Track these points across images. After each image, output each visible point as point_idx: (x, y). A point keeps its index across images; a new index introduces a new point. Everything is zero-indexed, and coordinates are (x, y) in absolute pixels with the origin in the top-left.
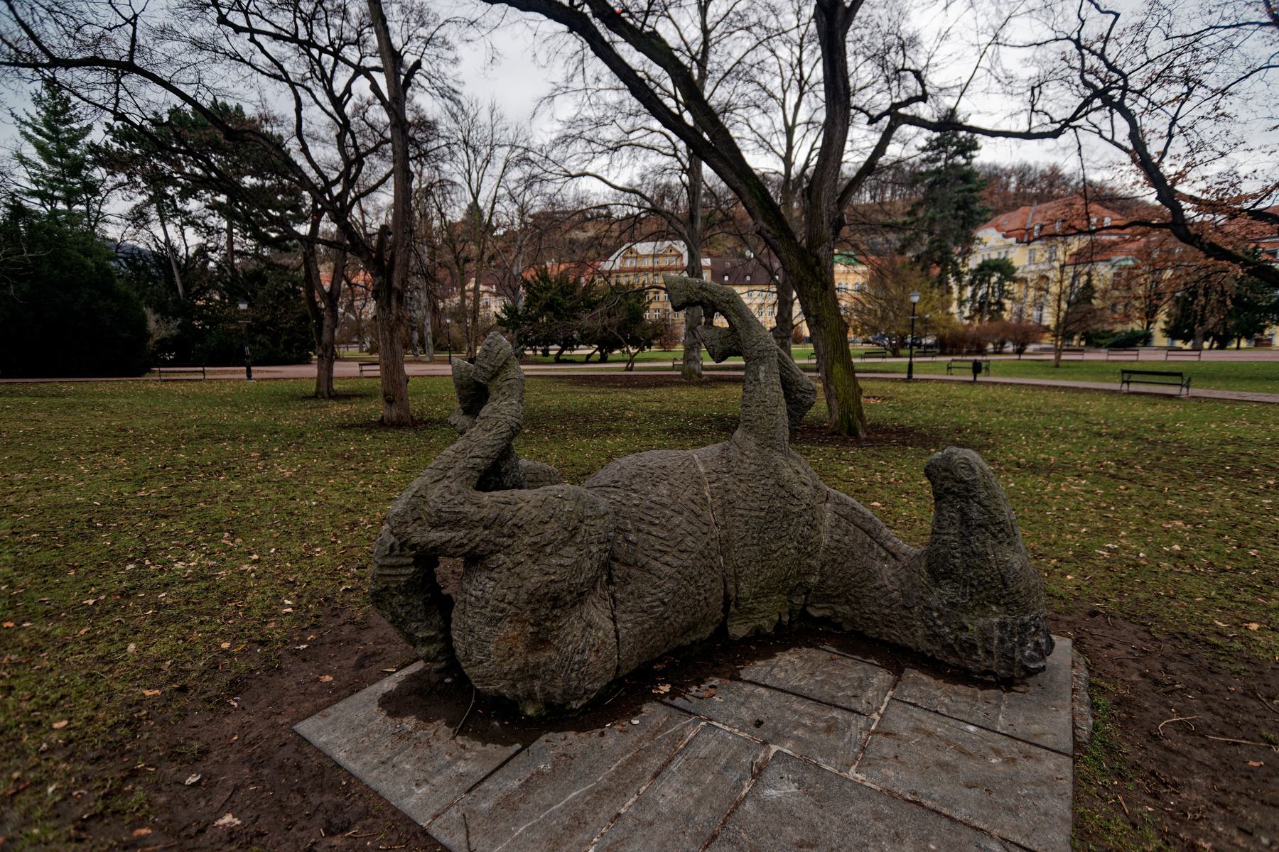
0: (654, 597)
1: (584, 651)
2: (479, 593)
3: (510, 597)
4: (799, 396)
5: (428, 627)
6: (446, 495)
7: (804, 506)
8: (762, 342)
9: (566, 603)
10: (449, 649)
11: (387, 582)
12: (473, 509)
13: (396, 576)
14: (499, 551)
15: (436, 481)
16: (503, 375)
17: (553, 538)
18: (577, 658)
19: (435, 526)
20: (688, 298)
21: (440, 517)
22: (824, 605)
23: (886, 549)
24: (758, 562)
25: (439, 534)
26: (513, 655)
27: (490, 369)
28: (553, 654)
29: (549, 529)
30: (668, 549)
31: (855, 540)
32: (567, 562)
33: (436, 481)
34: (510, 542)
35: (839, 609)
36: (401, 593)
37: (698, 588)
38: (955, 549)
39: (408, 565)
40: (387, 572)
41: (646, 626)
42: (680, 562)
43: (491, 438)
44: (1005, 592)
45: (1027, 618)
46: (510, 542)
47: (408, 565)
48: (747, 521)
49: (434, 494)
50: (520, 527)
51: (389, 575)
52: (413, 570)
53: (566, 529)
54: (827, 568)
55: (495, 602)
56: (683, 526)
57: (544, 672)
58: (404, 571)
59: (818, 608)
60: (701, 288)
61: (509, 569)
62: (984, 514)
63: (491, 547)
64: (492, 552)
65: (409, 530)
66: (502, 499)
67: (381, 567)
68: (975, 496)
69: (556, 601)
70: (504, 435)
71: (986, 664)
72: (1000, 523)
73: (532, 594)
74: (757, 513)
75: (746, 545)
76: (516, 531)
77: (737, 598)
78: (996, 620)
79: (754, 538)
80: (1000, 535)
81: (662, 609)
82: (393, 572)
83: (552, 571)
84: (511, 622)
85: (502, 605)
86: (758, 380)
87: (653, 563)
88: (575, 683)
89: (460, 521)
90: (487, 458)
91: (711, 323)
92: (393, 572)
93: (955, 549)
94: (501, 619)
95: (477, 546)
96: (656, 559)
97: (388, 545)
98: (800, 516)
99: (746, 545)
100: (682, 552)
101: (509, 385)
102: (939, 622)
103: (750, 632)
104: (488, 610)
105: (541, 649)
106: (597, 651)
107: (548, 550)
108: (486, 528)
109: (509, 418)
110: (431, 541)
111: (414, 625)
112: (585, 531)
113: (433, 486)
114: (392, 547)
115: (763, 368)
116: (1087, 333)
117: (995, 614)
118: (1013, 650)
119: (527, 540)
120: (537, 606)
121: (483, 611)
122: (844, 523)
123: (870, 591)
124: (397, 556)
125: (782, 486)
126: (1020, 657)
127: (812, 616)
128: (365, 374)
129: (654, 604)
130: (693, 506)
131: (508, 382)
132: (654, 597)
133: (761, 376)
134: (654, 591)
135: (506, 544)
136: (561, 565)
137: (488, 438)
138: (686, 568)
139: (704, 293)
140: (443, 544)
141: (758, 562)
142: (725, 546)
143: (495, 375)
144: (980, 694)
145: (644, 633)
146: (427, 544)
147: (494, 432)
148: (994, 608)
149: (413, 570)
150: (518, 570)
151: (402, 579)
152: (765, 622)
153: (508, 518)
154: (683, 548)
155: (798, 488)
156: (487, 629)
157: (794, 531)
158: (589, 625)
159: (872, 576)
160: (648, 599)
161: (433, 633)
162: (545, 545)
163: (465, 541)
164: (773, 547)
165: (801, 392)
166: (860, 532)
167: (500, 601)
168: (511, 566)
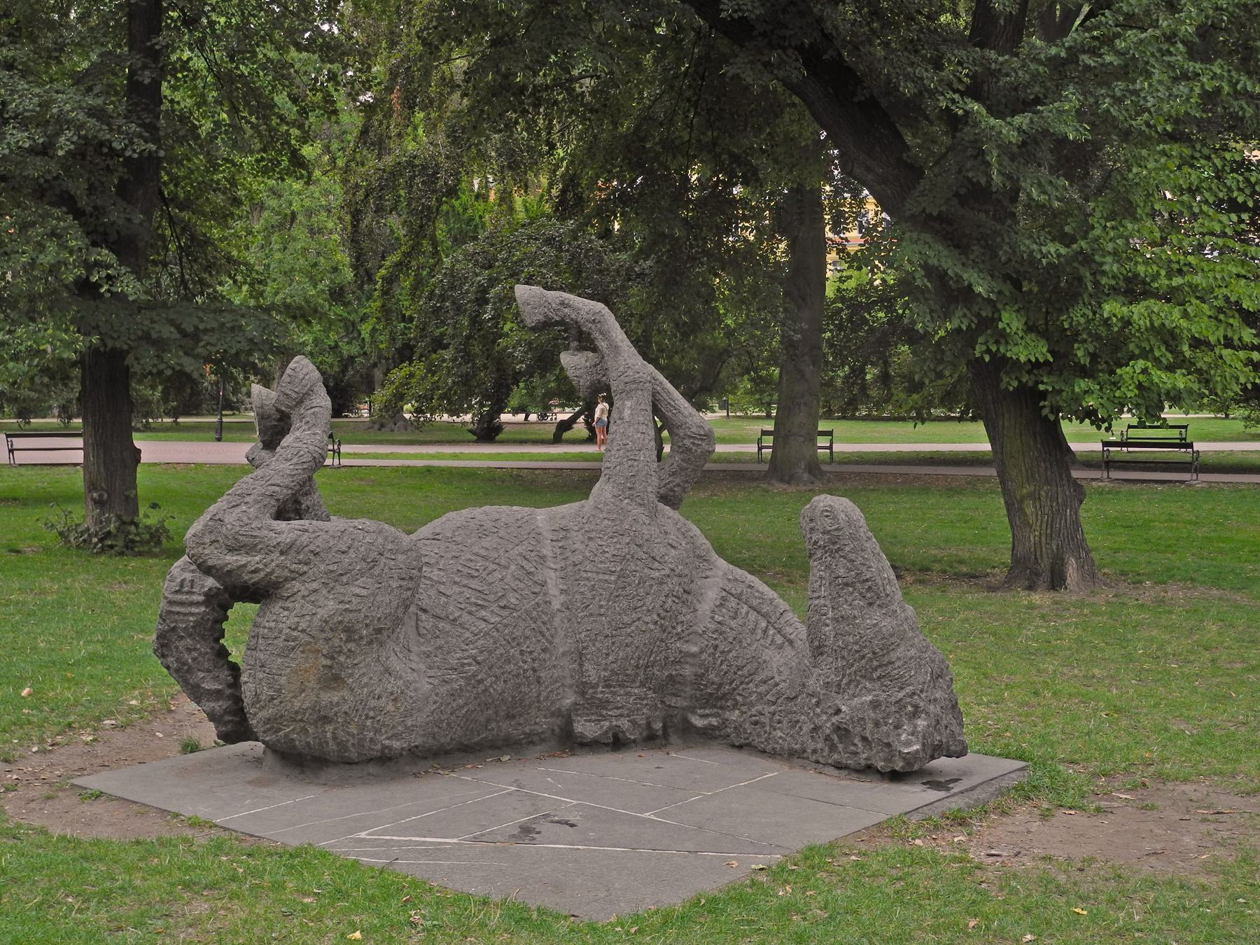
2: (272, 624)
3: (303, 625)
5: (216, 678)
6: (245, 519)
7: (667, 571)
8: (630, 372)
9: (361, 638)
10: (238, 700)
11: (176, 621)
13: (185, 614)
14: (294, 579)
15: (233, 506)
16: (307, 402)
18: (373, 703)
19: (231, 550)
23: (784, 636)
25: (235, 558)
26: (304, 691)
27: (294, 395)
28: (345, 693)
32: (364, 592)
33: (233, 506)
34: (305, 568)
36: (190, 635)
37: (522, 653)
39: (198, 604)
40: (177, 609)
44: (875, 663)
46: (305, 568)
47: (198, 604)
49: (230, 518)
50: (316, 554)
51: (178, 613)
52: (203, 609)
53: (364, 560)
55: (288, 630)
57: (336, 715)
59: (702, 716)
62: (850, 570)
63: (286, 573)
64: (287, 580)
72: (867, 580)
74: (607, 577)
75: (591, 615)
76: (312, 557)
78: (870, 698)
79: (601, 607)
81: (474, 668)
82: (182, 610)
84: (303, 652)
85: (295, 633)
89: (256, 545)
90: (286, 487)
92: (182, 610)
94: (293, 649)
95: (272, 572)
97: (179, 580)
101: (313, 413)
104: (281, 640)
105: (334, 689)
106: (395, 700)
107: (344, 579)
108: (282, 553)
109: (311, 448)
111: (201, 675)
114: (182, 584)
116: (1110, 375)
119: (322, 567)
120: (330, 635)
121: (275, 642)
122: (733, 603)
123: (757, 686)
125: (639, 546)
127: (695, 727)
128: (20, 457)
129: (466, 661)
130: (525, 563)
131: (313, 410)
132: (466, 654)
134: (465, 647)
137: (286, 467)
141: (607, 636)
143: (300, 402)
146: (222, 568)
147: (295, 460)
151: (191, 619)
152: (624, 723)
155: (659, 551)
156: (280, 660)
158: (388, 671)
159: (762, 665)
160: (458, 656)
161: (220, 687)
162: (342, 575)
163: (261, 566)
164: (626, 619)
165: (690, 437)
167: (294, 630)
168: (306, 593)
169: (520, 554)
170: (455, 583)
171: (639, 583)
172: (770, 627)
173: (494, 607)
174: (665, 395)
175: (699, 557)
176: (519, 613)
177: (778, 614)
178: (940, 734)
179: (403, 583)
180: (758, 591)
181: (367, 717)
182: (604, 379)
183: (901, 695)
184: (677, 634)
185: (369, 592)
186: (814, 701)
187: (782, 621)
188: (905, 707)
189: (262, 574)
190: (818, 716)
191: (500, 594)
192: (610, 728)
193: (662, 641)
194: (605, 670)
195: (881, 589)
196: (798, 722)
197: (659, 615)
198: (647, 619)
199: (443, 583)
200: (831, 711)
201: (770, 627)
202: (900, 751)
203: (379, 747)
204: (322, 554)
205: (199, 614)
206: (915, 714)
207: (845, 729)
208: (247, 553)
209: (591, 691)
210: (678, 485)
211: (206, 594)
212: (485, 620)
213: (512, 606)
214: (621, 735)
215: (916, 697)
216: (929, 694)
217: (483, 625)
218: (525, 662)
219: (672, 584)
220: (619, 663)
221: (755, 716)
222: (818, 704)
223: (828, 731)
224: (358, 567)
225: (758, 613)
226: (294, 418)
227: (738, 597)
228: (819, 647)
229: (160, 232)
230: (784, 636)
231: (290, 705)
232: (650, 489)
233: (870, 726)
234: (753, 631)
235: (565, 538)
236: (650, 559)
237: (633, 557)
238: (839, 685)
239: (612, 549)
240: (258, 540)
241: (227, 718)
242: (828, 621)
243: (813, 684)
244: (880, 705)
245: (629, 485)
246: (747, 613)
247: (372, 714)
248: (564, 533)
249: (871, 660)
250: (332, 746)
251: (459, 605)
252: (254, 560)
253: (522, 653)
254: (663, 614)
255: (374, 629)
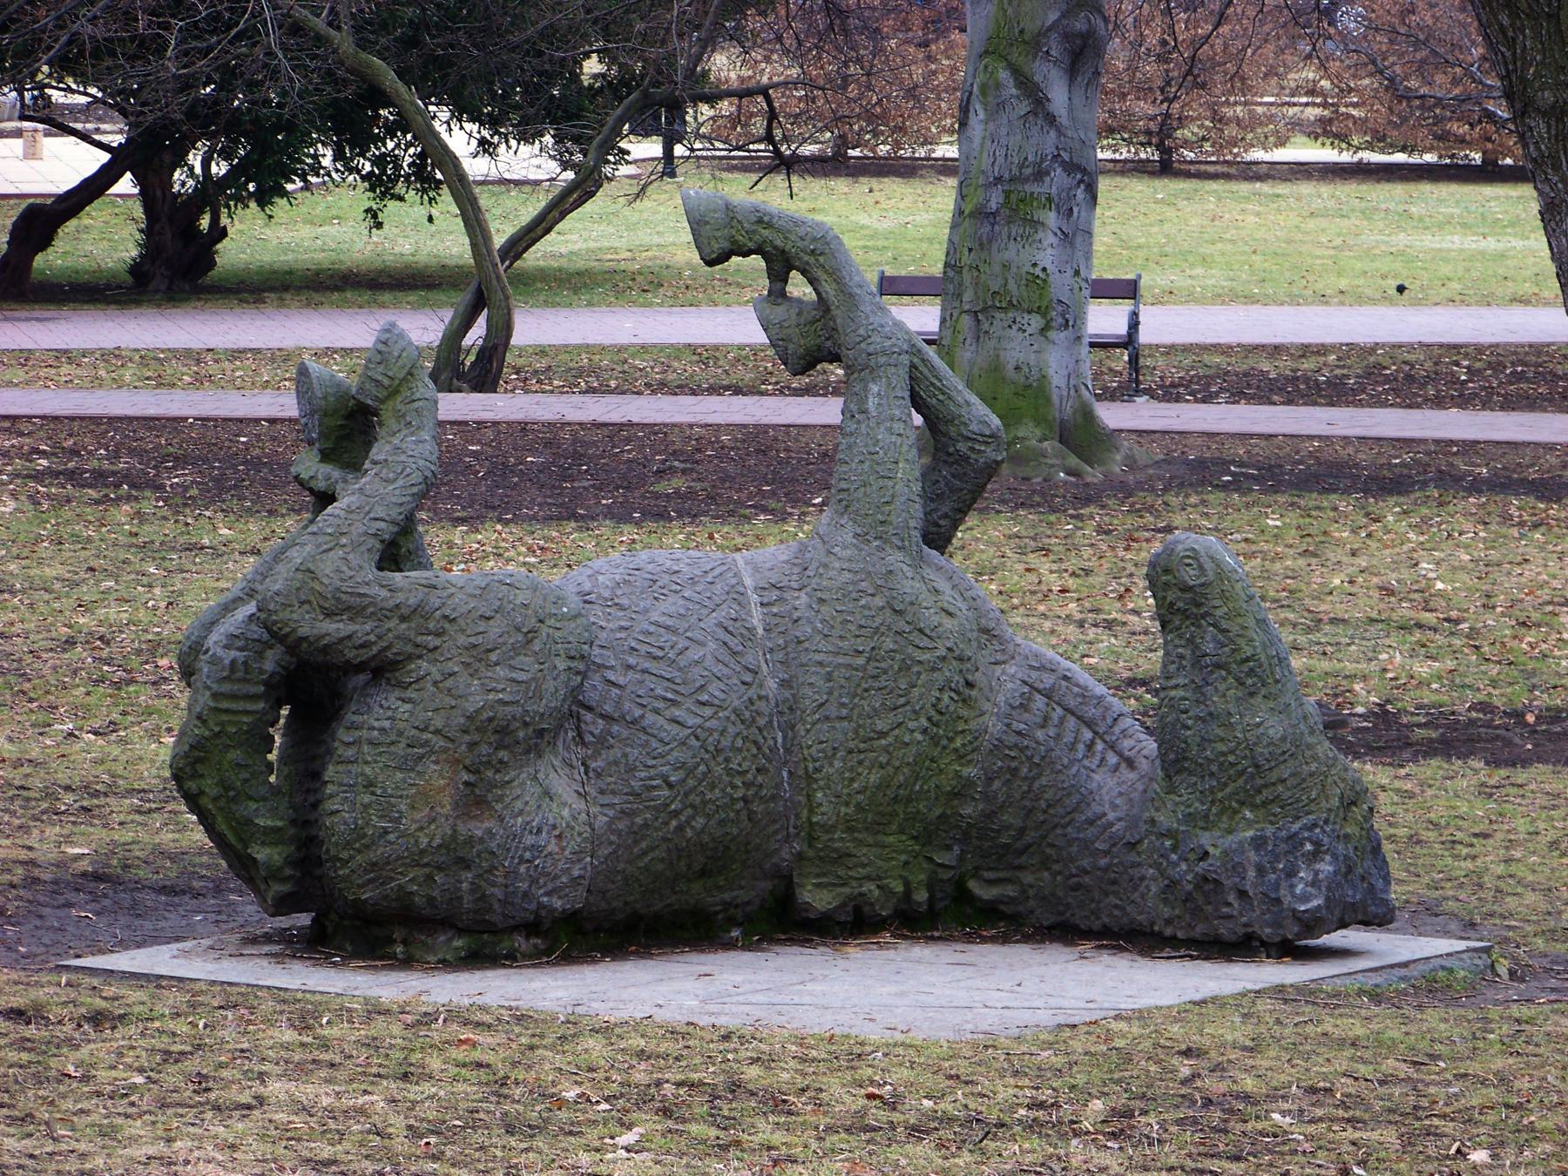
0: (652, 772)
1: (539, 831)
2: (387, 724)
3: (438, 722)
4: (962, 447)
7: (942, 652)
8: (876, 338)
12: (384, 593)
14: (420, 657)
15: (324, 551)
17: (500, 640)
18: (529, 840)
19: (329, 614)
20: (734, 242)
21: (338, 599)
22: (1001, 875)
23: (1120, 754)
24: (850, 752)
25: (335, 626)
26: (434, 820)
29: (495, 628)
30: (679, 698)
31: (1058, 737)
32: (522, 676)
34: (437, 642)
35: (1028, 878)
38: (1186, 712)
41: (639, 820)
42: (698, 721)
43: (397, 492)
44: (1259, 782)
45: (1296, 827)
46: (437, 642)
48: (829, 673)
51: (226, 711)
53: (518, 630)
54: (997, 784)
55: (414, 732)
56: (707, 663)
57: (478, 856)
58: (250, 706)
59: (990, 882)
60: (760, 221)
61: (435, 683)
63: (409, 649)
65: (295, 616)
66: (423, 582)
67: (215, 696)
68: (1207, 614)
69: (502, 733)
70: (415, 490)
71: (1244, 919)
72: (1247, 660)
73: (470, 718)
75: (827, 718)
76: (447, 626)
77: (811, 824)
78: (1250, 833)
79: (843, 705)
80: (1249, 682)
82: (234, 706)
83: (501, 686)
84: (436, 762)
86: (864, 412)
87: (650, 718)
88: (523, 886)
89: (364, 608)
91: (783, 294)
92: (234, 706)
93: (1186, 712)
94: (421, 757)
96: (657, 711)
98: (934, 669)
99: (827, 718)
100: (703, 704)
102: (1174, 857)
103: (843, 905)
106: (559, 837)
107: (493, 657)
108: (403, 619)
110: (323, 637)
112: (548, 635)
113: (324, 556)
115: (875, 388)
117: (1250, 824)
118: (1277, 887)
119: (462, 640)
120: (477, 737)
121: (393, 749)
122: (1039, 702)
124: (239, 680)
126: (1289, 898)
129: (654, 783)
130: (728, 638)
132: (652, 772)
133: (872, 403)
135: (431, 646)
136: (513, 680)
138: (711, 731)
139: (766, 233)
140: (341, 640)
141: (850, 752)
142: (789, 711)
144: (430, 295)
145: (637, 834)
147: (400, 483)
148: (1248, 814)
149: (261, 705)
150: (449, 683)
151: (245, 719)
152: (870, 888)
153: (437, 605)
154: (704, 697)
155: (931, 618)
156: (399, 775)
157: (921, 697)
160: (643, 774)
161: (280, 824)
163: (372, 638)
164: (881, 725)
166: (1071, 722)
167: (422, 730)
168: (439, 678)
169: (720, 625)
170: (629, 667)
171: (900, 669)
172: (1098, 741)
173: (689, 703)
174: (925, 371)
175: (986, 631)
176: (726, 713)
177: (1109, 721)
178: (1354, 887)
179: (573, 664)
180: (1077, 685)
181: (522, 860)
182: (829, 344)
183: (1296, 827)
184: (956, 750)
185: (530, 676)
186: (1168, 843)
187: (1117, 730)
188: (1302, 845)
189: (375, 650)
190: (1176, 864)
191: (698, 685)
192: (851, 898)
193: (932, 760)
194: (847, 804)
195: (1268, 672)
196: (1142, 878)
197: (929, 719)
198: (911, 725)
199: (612, 668)
200: (1192, 856)
201: (1098, 741)
202: (1294, 911)
203: (533, 906)
204: (459, 620)
205: (256, 712)
206: (1315, 856)
207: (1215, 880)
208: (351, 619)
209: (826, 837)
210: (946, 516)
211: (266, 683)
212: (678, 723)
213: (716, 702)
214: (866, 909)
215: (1317, 830)
216: (1338, 827)
217: (675, 729)
218: (734, 787)
219: (949, 671)
220: (868, 793)
221: (1075, 876)
222: (1174, 849)
223: (1190, 887)
224: (512, 641)
225: (1078, 718)
226: (386, 413)
227: (1048, 694)
228: (1177, 761)
229: (1530, 718)
230: (1120, 754)
231: (412, 841)
232: (912, 523)
233: (1252, 874)
234: (1072, 747)
235: (780, 599)
236: (916, 633)
237: (889, 629)
238: (1206, 816)
239: (858, 616)
240: (367, 601)
241: (288, 872)
242: (1190, 722)
243: (1164, 819)
244: (1266, 843)
245: (880, 517)
246: (1062, 720)
247: (528, 855)
248: (777, 592)
249: (1252, 776)
250: (467, 902)
251: (638, 700)
252: (362, 629)
253: (729, 771)
254: (936, 717)
255: (534, 730)
